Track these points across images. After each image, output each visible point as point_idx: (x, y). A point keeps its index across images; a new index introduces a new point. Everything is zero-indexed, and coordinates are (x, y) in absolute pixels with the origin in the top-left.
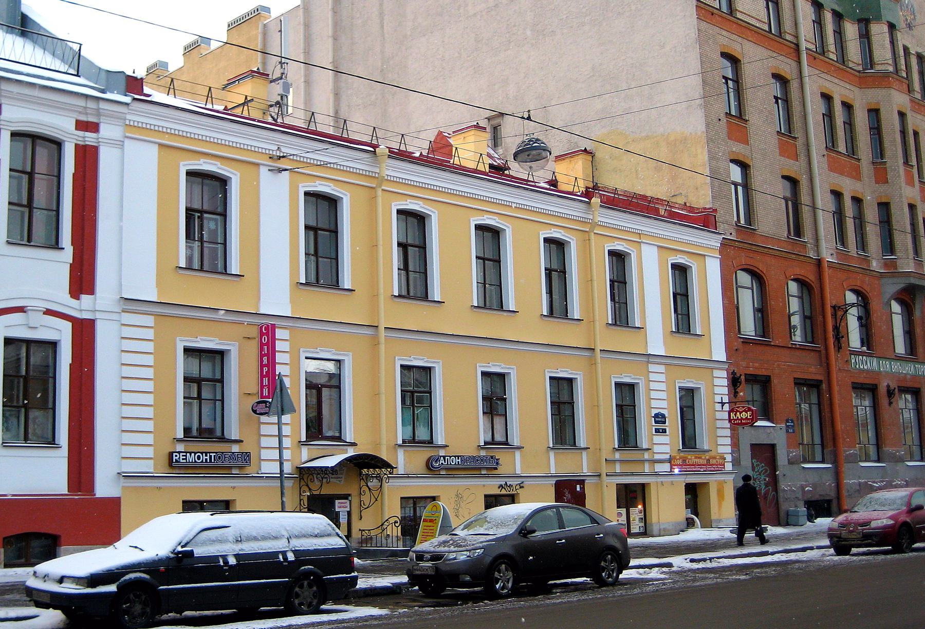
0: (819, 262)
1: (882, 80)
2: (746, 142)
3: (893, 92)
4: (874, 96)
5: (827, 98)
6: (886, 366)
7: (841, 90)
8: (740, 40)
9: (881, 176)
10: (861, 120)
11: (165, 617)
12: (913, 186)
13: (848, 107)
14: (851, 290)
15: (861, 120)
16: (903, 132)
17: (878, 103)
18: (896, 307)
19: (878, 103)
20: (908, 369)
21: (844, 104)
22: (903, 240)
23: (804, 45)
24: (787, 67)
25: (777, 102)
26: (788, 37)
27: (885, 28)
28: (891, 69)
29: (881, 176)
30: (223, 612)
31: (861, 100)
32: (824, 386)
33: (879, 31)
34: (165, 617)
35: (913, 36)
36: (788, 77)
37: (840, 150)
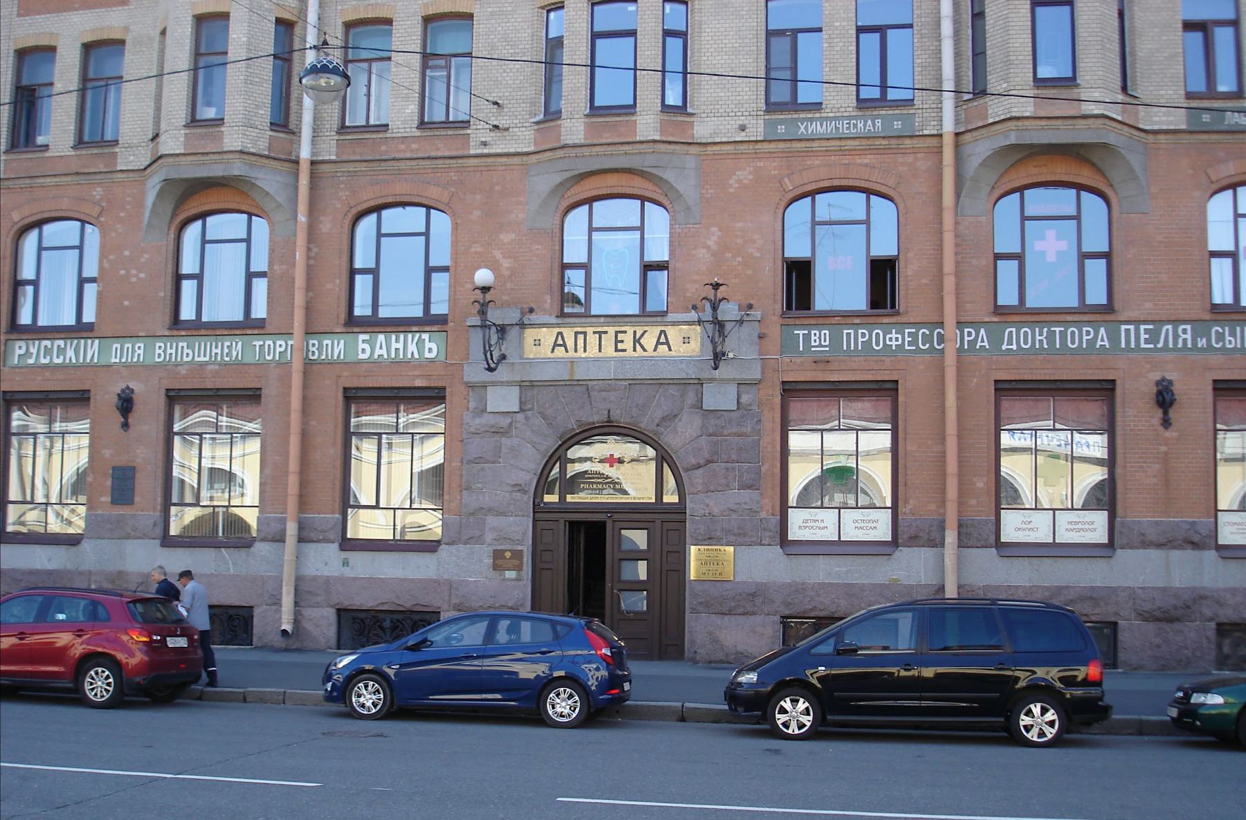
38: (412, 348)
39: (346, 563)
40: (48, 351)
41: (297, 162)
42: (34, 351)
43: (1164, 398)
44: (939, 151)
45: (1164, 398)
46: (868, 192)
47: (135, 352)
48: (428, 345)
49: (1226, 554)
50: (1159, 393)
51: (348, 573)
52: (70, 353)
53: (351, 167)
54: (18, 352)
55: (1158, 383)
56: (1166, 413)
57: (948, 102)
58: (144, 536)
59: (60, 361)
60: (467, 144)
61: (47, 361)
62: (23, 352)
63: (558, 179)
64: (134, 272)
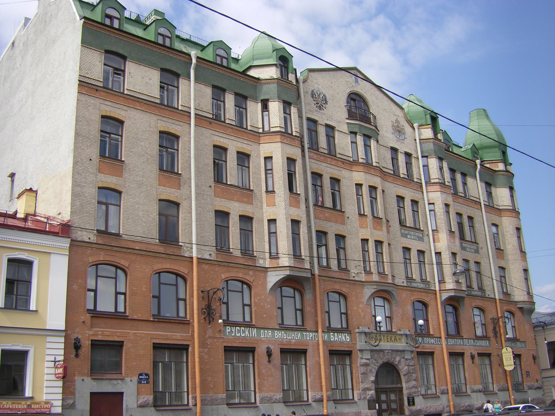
17: (271, 153)
19: (271, 153)
32: (190, 349)
38: (344, 338)
39: (336, 408)
40: (239, 331)
41: (192, 258)
42: (234, 330)
43: (269, 354)
44: (436, 294)
45: (269, 354)
46: (117, 267)
47: (266, 335)
48: (347, 337)
49: (336, 402)
50: (75, 343)
51: (337, 411)
52: (247, 333)
53: (324, 278)
54: (228, 331)
55: (75, 339)
56: (77, 351)
57: (194, 247)
58: (279, 402)
59: (244, 335)
60: (387, 280)
61: (239, 335)
62: (229, 330)
63: (373, 291)
64: (266, 304)
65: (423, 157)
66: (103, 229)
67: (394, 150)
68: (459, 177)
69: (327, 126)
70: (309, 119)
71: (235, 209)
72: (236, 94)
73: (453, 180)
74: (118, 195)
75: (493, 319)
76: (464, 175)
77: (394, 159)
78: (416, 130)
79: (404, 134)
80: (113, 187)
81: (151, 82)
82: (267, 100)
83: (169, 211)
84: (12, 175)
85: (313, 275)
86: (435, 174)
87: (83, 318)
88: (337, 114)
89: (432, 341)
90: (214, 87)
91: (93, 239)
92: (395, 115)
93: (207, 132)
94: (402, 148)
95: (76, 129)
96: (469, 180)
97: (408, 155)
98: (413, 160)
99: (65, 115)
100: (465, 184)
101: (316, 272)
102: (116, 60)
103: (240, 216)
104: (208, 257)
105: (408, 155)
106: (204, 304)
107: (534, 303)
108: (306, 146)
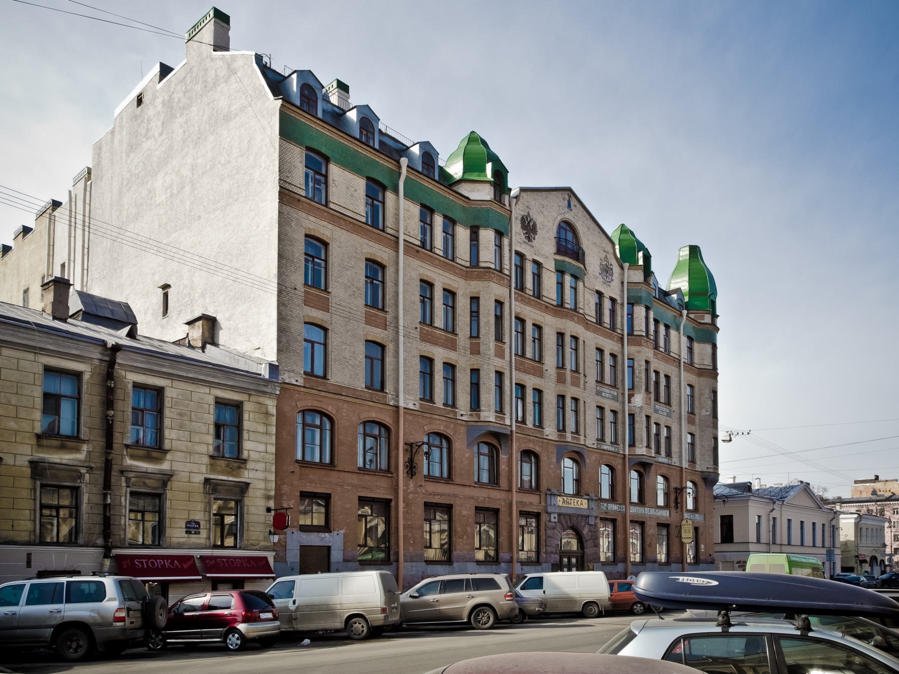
0: (397, 407)
1: (485, 274)
2: (327, 309)
3: (493, 285)
4: (475, 287)
5: (600, 351)
6: (653, 512)
7: (610, 346)
8: (330, 226)
9: (475, 350)
10: (463, 305)
11: (129, 651)
12: (503, 358)
13: (538, 327)
14: (607, 465)
15: (463, 305)
16: (647, 370)
17: (479, 293)
18: (634, 475)
19: (479, 293)
20: (665, 513)
21: (611, 354)
22: (488, 396)
23: (683, 360)
24: (383, 254)
25: (534, 341)
26: (389, 231)
27: (644, 309)
28: (644, 334)
29: (475, 350)
30: (759, 600)
31: (464, 289)
32: (393, 504)
33: (487, 236)
34: (129, 651)
35: (532, 247)
36: (384, 263)
37: (606, 382)
65: (628, 304)
66: (309, 370)
67: (600, 294)
68: (662, 329)
69: (535, 262)
70: (517, 253)
71: (440, 355)
72: (445, 217)
73: (656, 331)
74: (322, 332)
75: (676, 489)
76: (667, 327)
77: (599, 306)
78: (626, 270)
79: (612, 275)
80: (319, 323)
81: (356, 194)
82: (472, 266)
83: (377, 352)
84: (166, 287)
85: (511, 431)
86: (640, 326)
87: (291, 469)
88: (544, 249)
89: (554, 460)
90: (423, 206)
91: (301, 382)
92: (605, 251)
93: (415, 263)
94: (608, 292)
95: (279, 250)
96: (673, 333)
97: (613, 300)
98: (618, 307)
99: (258, 227)
100: (667, 335)
101: (514, 429)
102: (318, 163)
103: (444, 363)
104: (412, 407)
105: (613, 300)
106: (408, 456)
107: (718, 475)
108: (513, 285)
